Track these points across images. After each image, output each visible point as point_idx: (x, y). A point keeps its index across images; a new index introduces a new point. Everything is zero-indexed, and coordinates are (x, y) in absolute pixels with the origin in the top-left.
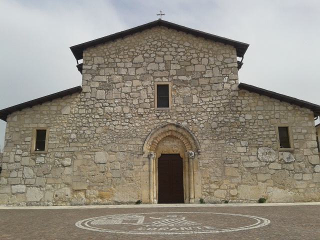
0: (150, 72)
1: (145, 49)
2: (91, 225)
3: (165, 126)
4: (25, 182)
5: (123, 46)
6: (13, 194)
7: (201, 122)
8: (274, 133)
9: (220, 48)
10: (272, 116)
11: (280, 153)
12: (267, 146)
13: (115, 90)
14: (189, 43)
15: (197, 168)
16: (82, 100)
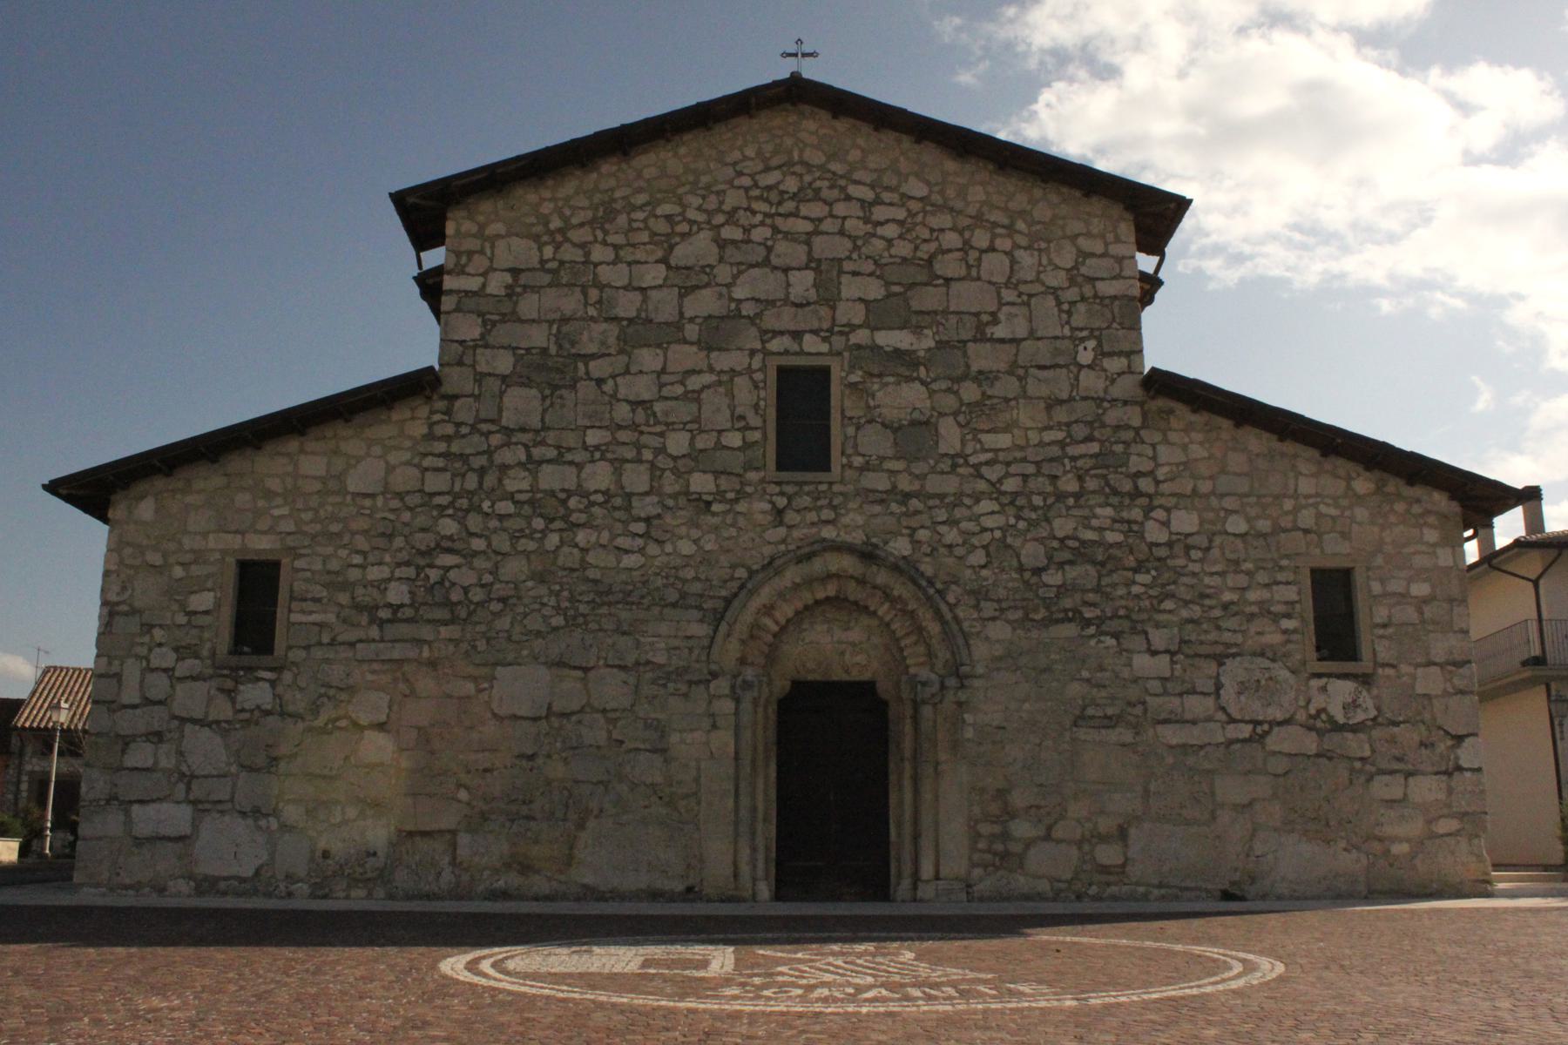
0: (748, 309)
1: (726, 207)
2: (508, 973)
3: (809, 557)
4: (189, 789)
5: (627, 191)
6: (139, 842)
7: (975, 541)
8: (1291, 593)
9: (1064, 210)
10: (1286, 522)
11: (1315, 683)
12: (1262, 655)
13: (586, 389)
14: (928, 183)
15: (955, 745)
16: (439, 430)
